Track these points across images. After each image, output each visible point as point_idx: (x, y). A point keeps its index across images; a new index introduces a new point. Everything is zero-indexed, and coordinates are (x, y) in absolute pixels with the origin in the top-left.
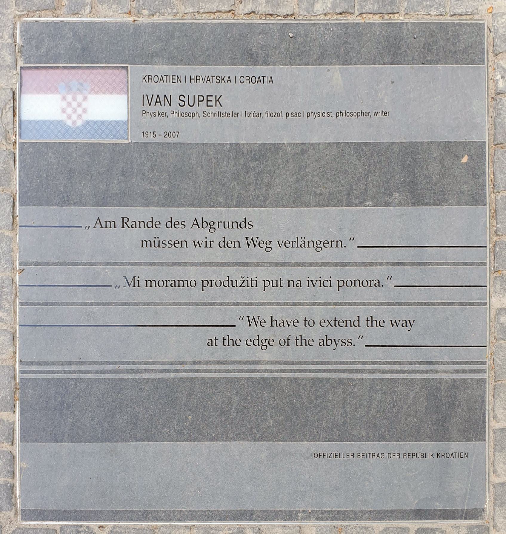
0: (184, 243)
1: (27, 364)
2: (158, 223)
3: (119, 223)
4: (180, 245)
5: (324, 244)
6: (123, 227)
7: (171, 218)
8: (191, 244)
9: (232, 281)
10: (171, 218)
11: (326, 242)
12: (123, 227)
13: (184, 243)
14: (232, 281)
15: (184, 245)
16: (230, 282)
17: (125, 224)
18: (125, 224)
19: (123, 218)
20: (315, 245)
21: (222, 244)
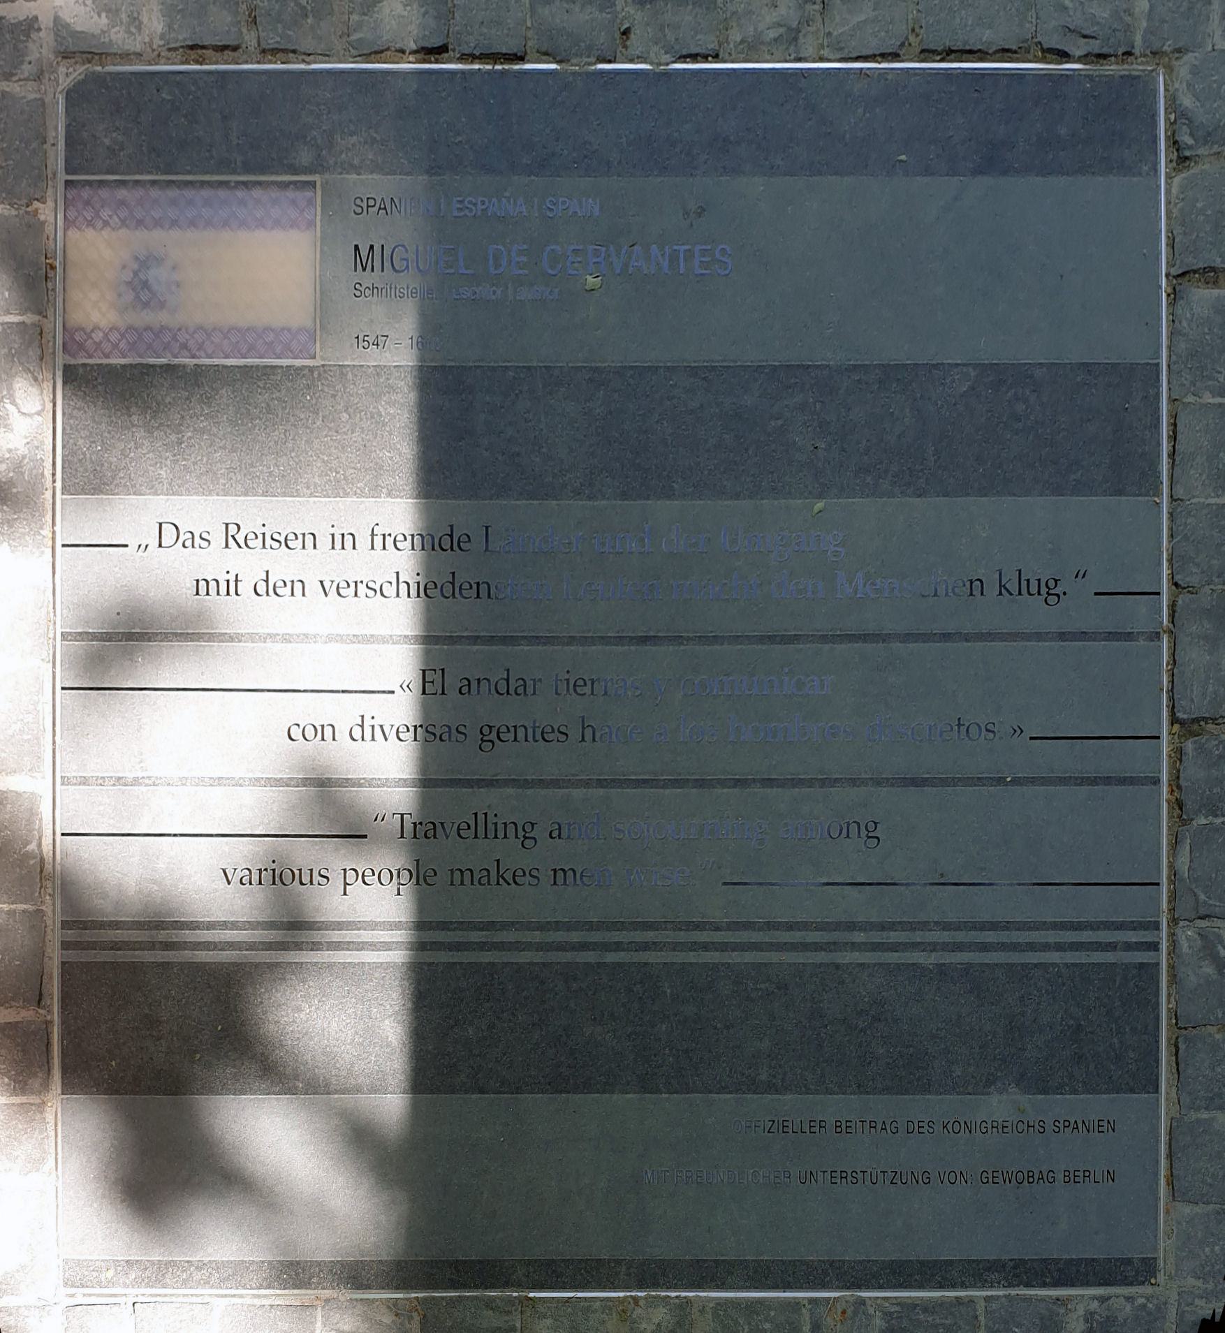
0: (298, 586)
1: (444, 926)
2: (464, 538)
3: (218, 538)
4: (474, 592)
5: (498, 733)
6: (227, 546)
7: (452, 526)
8: (313, 587)
9: (1028, 581)
10: (452, 526)
11: (503, 729)
12: (227, 546)
13: (298, 586)
14: (1028, 581)
15: (483, 593)
16: (1024, 584)
17: (230, 539)
18: (230, 539)
19: (227, 525)
20: (521, 834)
21: (261, 588)
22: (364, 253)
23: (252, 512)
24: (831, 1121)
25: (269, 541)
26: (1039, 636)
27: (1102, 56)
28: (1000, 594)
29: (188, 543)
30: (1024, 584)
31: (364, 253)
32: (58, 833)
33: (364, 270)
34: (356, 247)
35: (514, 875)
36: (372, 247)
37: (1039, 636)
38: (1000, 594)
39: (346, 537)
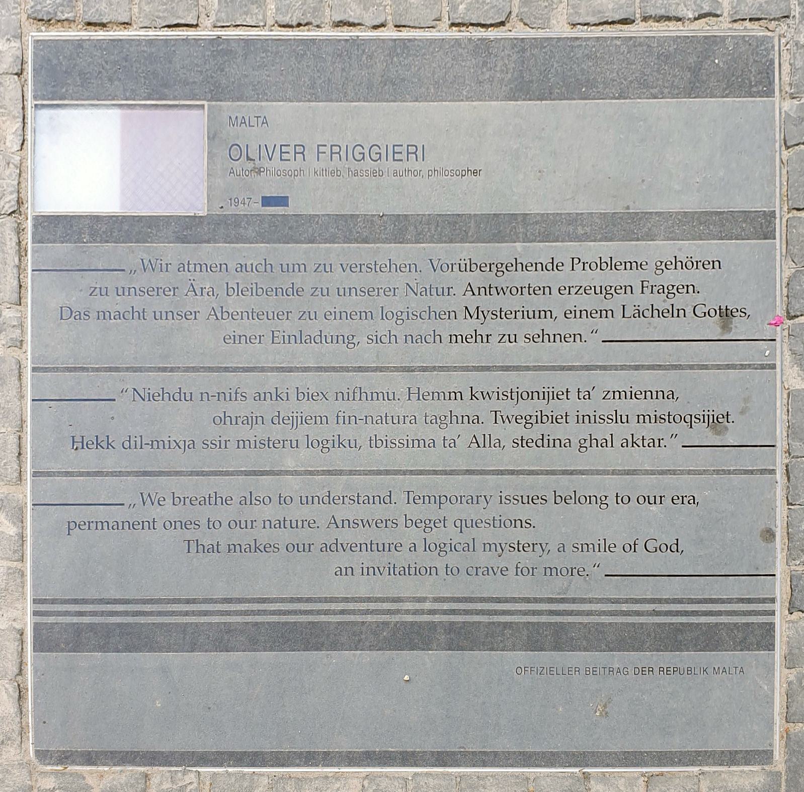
9: (621, 416)
14: (621, 416)
22: (233, 119)
23: (491, 587)
24: (175, 263)
25: (501, 396)
26: (306, 369)
27: (102, 443)
28: (472, 399)
29: (77, 317)
30: (619, 418)
31: (233, 119)
32: (143, 443)
33: (233, 125)
34: (230, 117)
35: (265, 548)
36: (237, 117)
37: (306, 369)
38: (472, 399)
39: (286, 270)
